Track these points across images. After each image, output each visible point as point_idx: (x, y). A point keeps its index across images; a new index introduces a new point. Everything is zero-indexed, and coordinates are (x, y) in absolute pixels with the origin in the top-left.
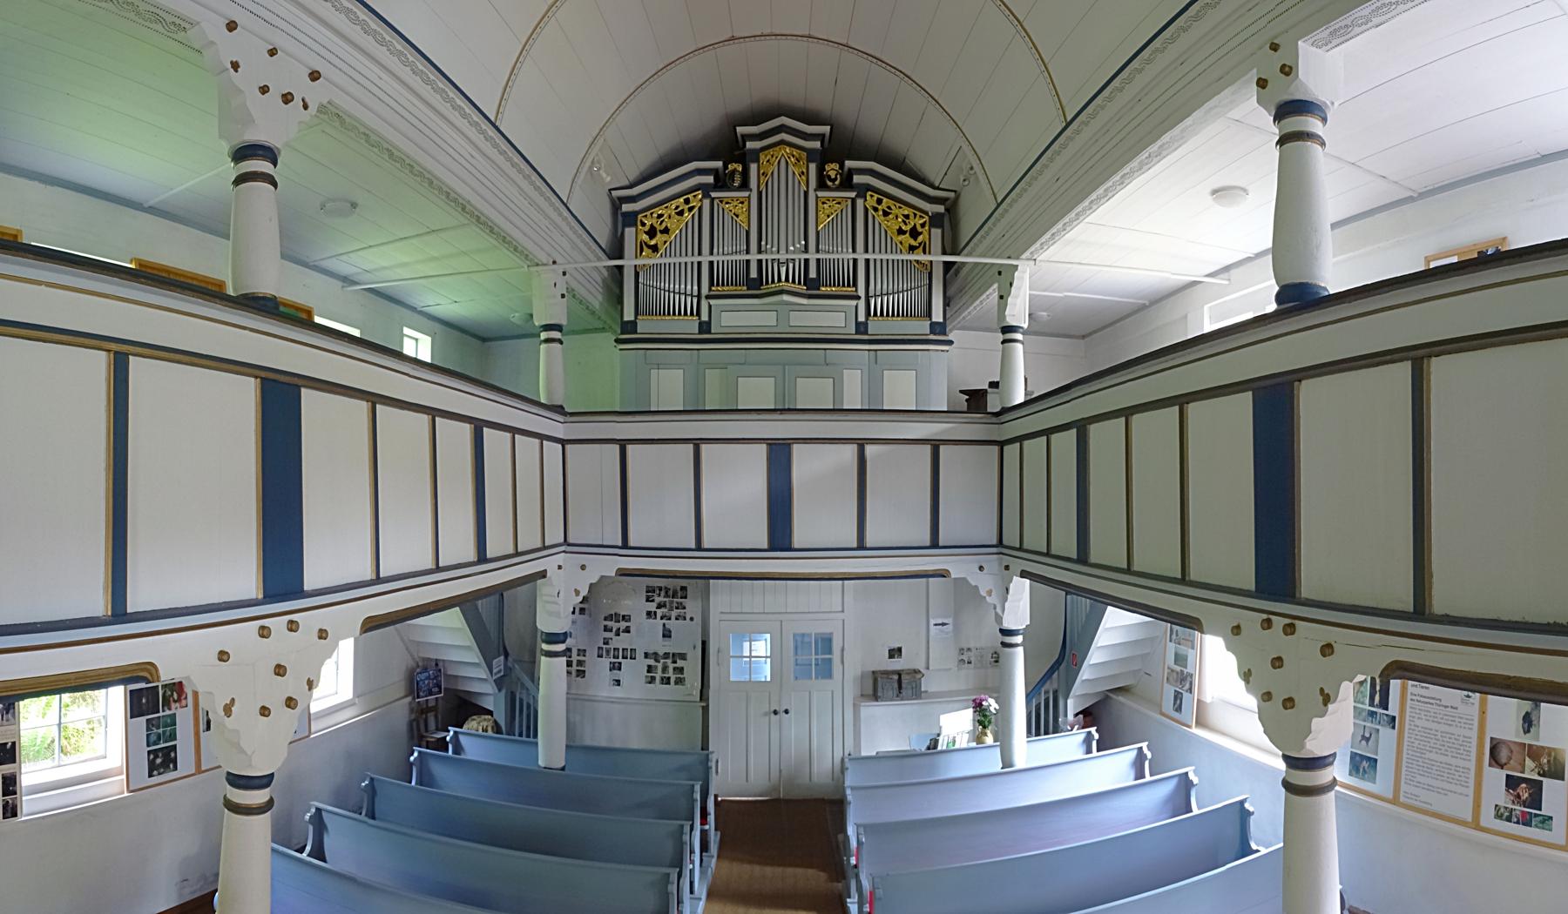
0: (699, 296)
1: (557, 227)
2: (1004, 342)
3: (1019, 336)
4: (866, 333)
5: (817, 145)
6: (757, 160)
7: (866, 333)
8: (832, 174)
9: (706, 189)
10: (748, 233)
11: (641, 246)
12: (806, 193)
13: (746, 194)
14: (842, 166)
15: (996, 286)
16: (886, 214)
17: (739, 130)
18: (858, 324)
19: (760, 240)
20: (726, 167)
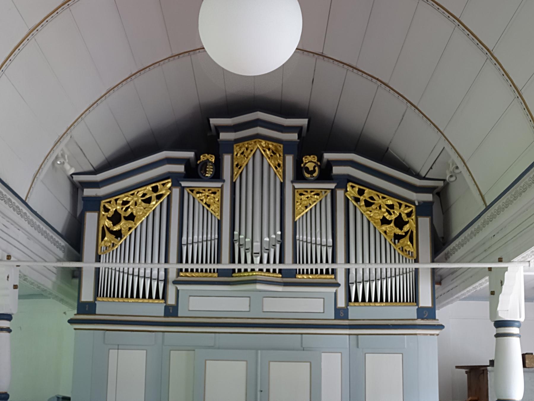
0: (166, 281)
1: (14, 223)
2: (497, 335)
3: (514, 330)
4: (346, 318)
5: (294, 137)
6: (231, 152)
7: (346, 318)
8: (310, 166)
9: (176, 179)
10: (220, 222)
11: (104, 232)
12: (282, 185)
13: (219, 185)
14: (320, 159)
15: (487, 278)
16: (368, 204)
17: (214, 121)
18: (337, 310)
19: (233, 229)
20: (197, 157)
